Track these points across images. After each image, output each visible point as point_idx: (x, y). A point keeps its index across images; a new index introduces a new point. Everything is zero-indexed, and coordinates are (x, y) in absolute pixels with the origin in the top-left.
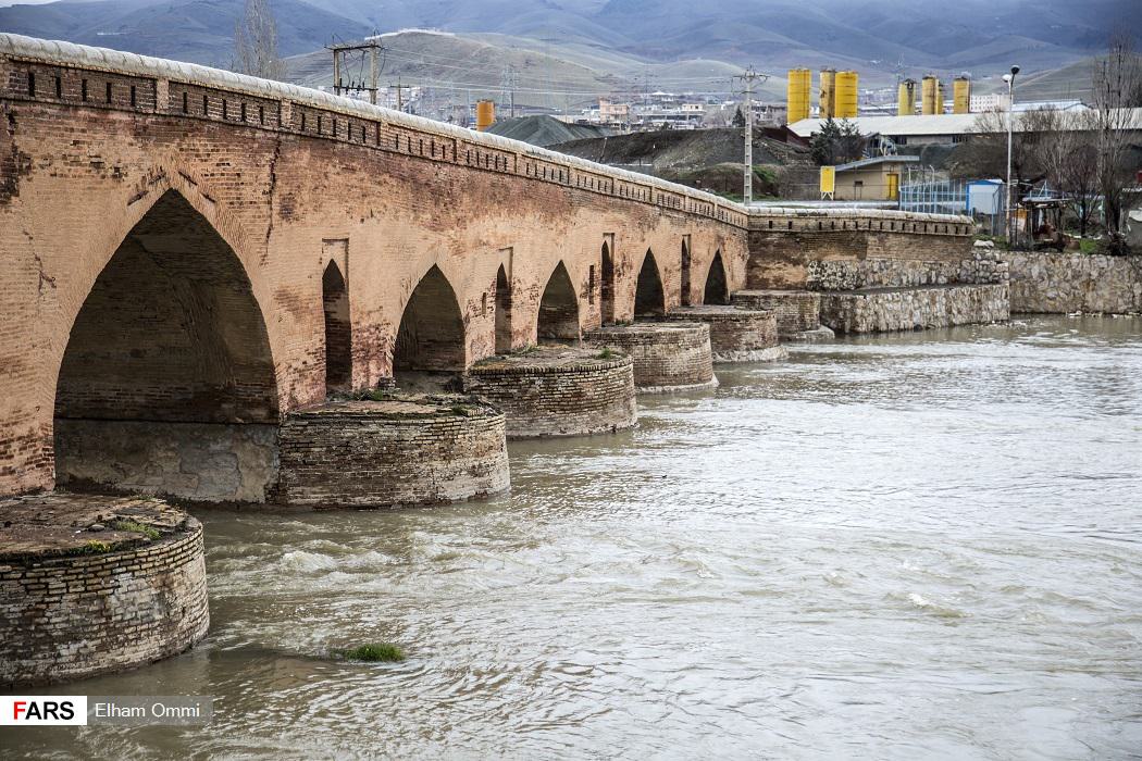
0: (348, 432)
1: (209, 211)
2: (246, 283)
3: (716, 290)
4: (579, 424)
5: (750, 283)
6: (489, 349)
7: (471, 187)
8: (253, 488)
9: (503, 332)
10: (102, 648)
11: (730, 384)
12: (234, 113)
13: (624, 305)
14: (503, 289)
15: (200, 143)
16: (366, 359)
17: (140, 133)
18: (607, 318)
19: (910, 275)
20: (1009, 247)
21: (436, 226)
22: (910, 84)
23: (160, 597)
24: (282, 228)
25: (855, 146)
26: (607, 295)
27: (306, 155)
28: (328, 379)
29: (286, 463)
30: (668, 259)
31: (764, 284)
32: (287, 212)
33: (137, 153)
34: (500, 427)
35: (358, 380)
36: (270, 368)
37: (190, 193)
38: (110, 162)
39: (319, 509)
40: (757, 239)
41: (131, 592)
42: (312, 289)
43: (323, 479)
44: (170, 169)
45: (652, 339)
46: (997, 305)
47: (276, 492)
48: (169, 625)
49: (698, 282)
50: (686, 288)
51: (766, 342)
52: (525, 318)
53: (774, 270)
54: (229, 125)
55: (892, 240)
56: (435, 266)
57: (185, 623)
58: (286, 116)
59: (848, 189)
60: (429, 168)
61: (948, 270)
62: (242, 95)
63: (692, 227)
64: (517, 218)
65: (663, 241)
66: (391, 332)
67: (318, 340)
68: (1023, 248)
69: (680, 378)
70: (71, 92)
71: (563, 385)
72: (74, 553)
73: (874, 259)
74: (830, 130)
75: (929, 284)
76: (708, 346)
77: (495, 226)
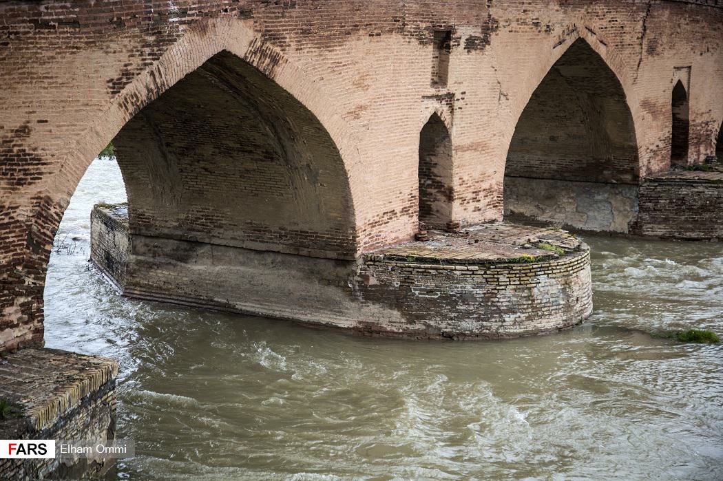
1: (602, 51)
2: (623, 96)
10: (529, 318)
23: (564, 290)
24: (649, 60)
29: (642, 209)
32: (652, 51)
36: (635, 149)
41: (546, 286)
42: (664, 98)
43: (666, 220)
47: (636, 227)
48: (568, 307)
57: (578, 307)
67: (667, 132)
72: (514, 261)
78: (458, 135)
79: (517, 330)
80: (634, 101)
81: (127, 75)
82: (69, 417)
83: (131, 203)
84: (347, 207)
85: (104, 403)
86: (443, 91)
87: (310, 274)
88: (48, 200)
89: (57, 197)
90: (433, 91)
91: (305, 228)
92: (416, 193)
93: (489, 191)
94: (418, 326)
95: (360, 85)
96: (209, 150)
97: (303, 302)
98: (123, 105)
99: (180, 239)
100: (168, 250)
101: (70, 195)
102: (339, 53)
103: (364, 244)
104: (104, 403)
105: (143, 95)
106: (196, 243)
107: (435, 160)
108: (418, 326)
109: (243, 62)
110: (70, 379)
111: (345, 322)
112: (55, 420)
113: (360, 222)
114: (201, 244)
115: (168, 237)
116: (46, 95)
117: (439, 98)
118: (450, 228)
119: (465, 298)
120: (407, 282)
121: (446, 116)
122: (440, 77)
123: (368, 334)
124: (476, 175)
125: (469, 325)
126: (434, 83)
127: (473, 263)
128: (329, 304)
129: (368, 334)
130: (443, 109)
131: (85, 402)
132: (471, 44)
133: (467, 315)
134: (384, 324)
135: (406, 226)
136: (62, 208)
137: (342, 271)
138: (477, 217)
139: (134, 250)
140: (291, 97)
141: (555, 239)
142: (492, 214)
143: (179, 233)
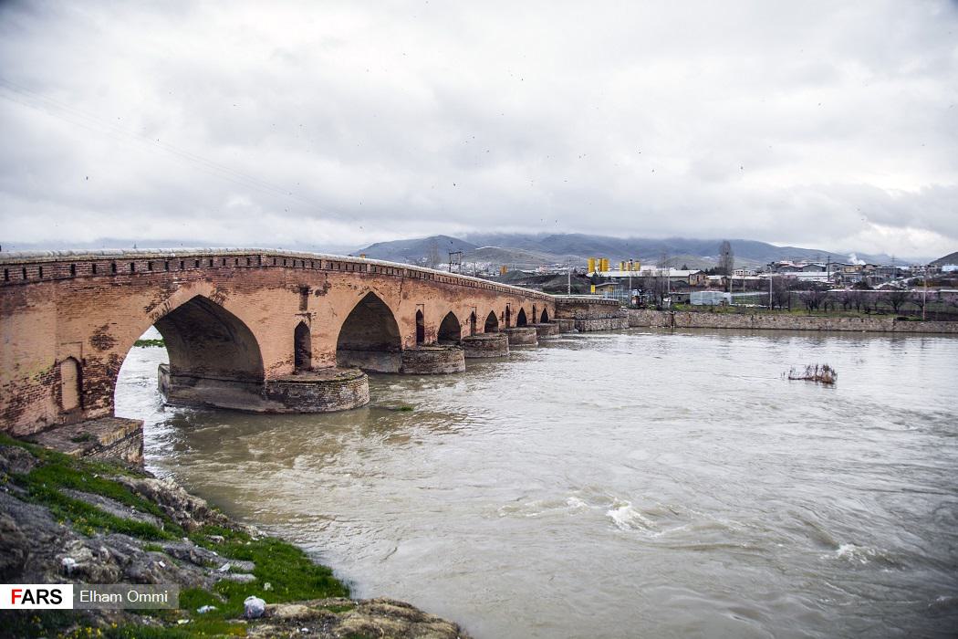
0: (420, 355)
1: (382, 297)
2: (393, 316)
3: (545, 318)
4: (492, 354)
5: (556, 317)
6: (469, 334)
7: (463, 290)
8: (395, 369)
9: (473, 330)
10: (338, 405)
11: (543, 344)
12: (390, 272)
13: (513, 322)
14: (473, 317)
15: (379, 280)
16: (429, 336)
17: (362, 277)
18: (508, 326)
19: (601, 315)
20: (630, 308)
21: (451, 301)
22: (623, 263)
23: (354, 393)
24: (404, 302)
25: (602, 279)
26: (508, 320)
27: (411, 282)
28: (417, 341)
29: (404, 362)
30: (528, 310)
31: (560, 317)
32: (405, 297)
33: (361, 282)
34: (462, 353)
35: (426, 341)
36: (400, 337)
37: (376, 292)
38: (353, 285)
39: (412, 374)
40: (558, 305)
41: (345, 391)
42: (413, 317)
43: (413, 367)
44: (371, 286)
45: (519, 332)
46: (625, 324)
47: (401, 370)
48: (356, 400)
49: (538, 316)
50: (534, 318)
51: (556, 333)
52: (480, 325)
53: (563, 313)
54: (388, 275)
55: (596, 306)
56: (451, 312)
57: (360, 400)
58: (405, 273)
59: (598, 292)
60: (449, 286)
61: (612, 314)
62: (392, 267)
63: (536, 302)
64: (478, 299)
65: (527, 306)
66: (437, 329)
67: (414, 330)
68: (634, 308)
69: (526, 343)
70: (343, 267)
71: (487, 344)
72: (332, 381)
73: (591, 311)
74: (595, 275)
75: (607, 318)
76: (535, 334)
77: (471, 301)
78: (314, 329)
79: (333, 410)
80: (398, 318)
81: (153, 305)
82: (120, 441)
83: (171, 365)
84: (260, 361)
85: (137, 438)
86: (305, 312)
87: (246, 390)
88: (116, 356)
89: (120, 355)
90: (301, 312)
91: (244, 370)
92: (293, 355)
93: (329, 354)
94: (291, 410)
95: (265, 309)
96: (202, 338)
97: (243, 401)
98: (152, 317)
99: (192, 377)
100: (186, 381)
101: (126, 353)
102: (254, 296)
103: (268, 376)
104: (137, 438)
105: (161, 313)
106: (198, 378)
107: (303, 341)
108: (291, 410)
109: (208, 299)
110: (121, 427)
111: (260, 410)
112: (112, 442)
113: (265, 367)
114: (200, 378)
115: (187, 376)
116: (116, 313)
117: (303, 315)
118: (310, 370)
119: (311, 397)
120: (286, 391)
121: (307, 323)
122: (304, 306)
123: (270, 413)
124: (322, 347)
125: (312, 408)
126: (301, 309)
127: (314, 382)
128: (253, 402)
129: (270, 413)
130: (306, 320)
131: (127, 437)
132: (318, 293)
133: (312, 404)
134: (277, 409)
135: (286, 370)
136: (123, 359)
137: (259, 388)
138: (324, 365)
139: (172, 382)
140: (231, 313)
141: (351, 373)
142: (330, 364)
143: (190, 374)
